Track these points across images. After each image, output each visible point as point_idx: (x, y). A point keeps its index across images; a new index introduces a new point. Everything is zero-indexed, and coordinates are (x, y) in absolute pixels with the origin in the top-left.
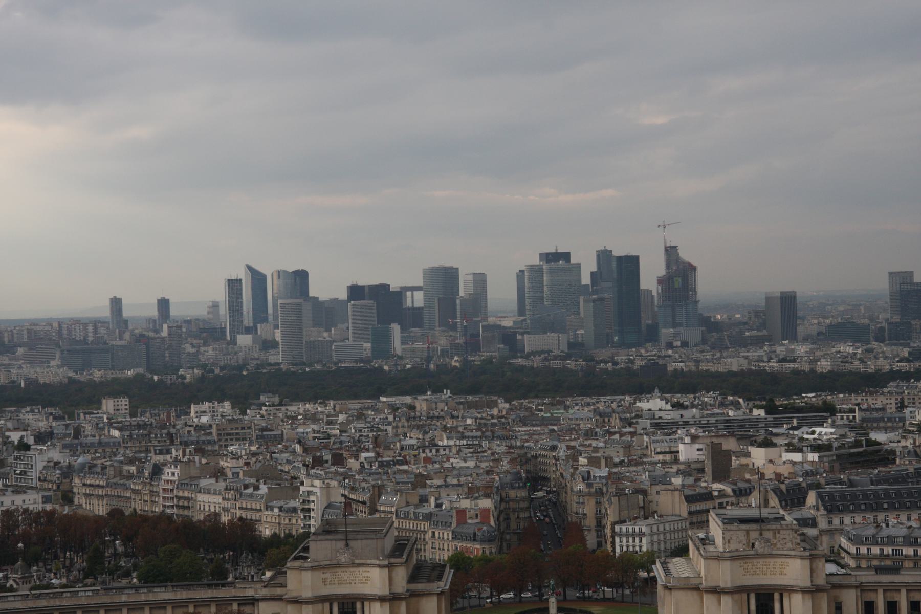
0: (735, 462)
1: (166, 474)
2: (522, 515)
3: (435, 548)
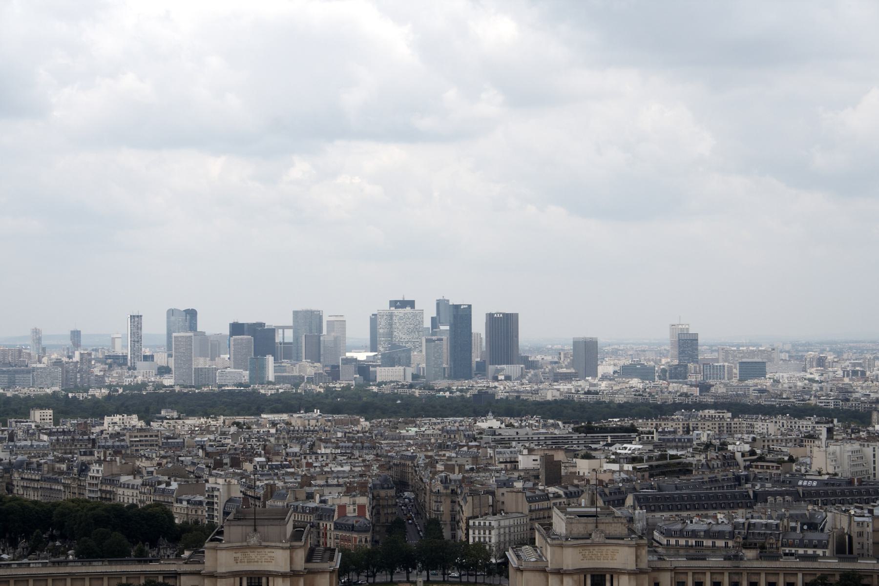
1: (92, 471)
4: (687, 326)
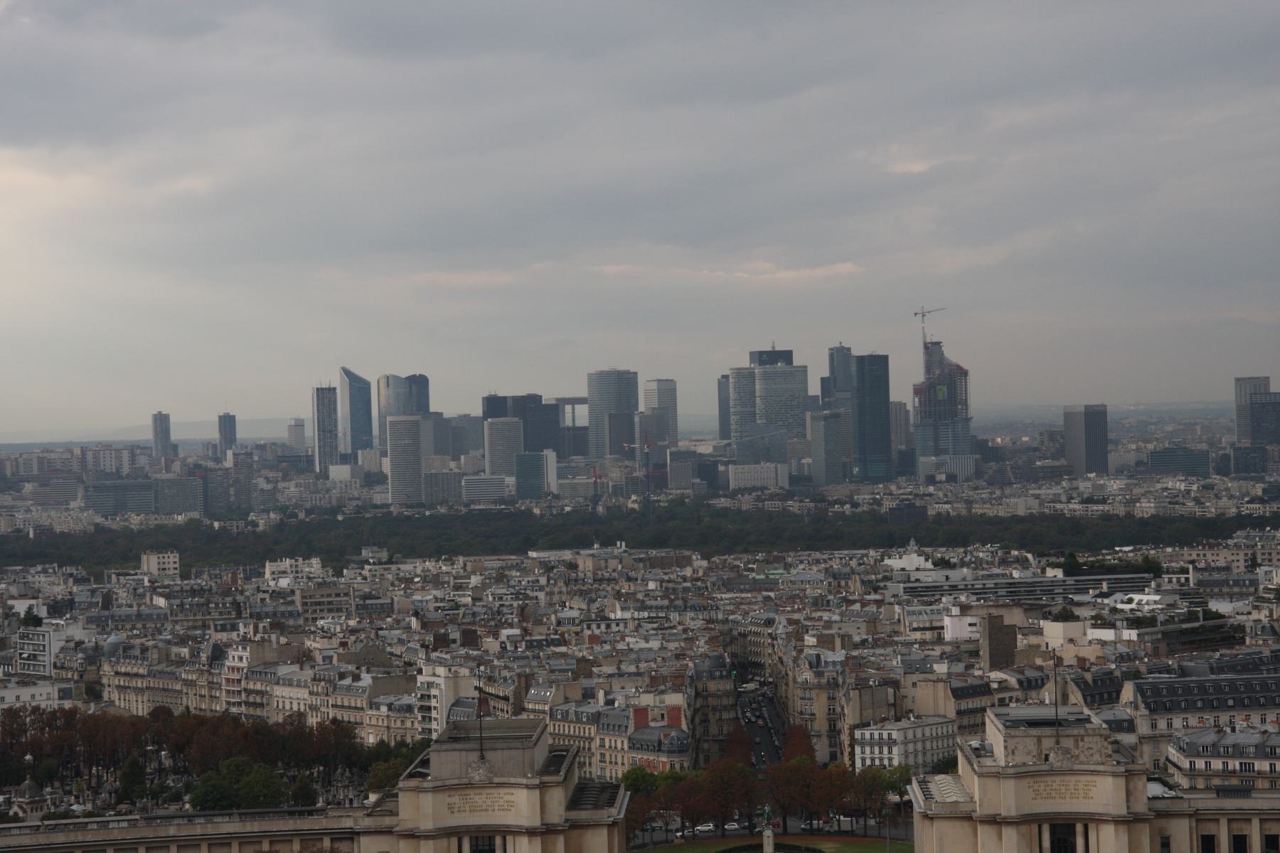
0: (1021, 642)
1: (231, 658)
2: (725, 716)
3: (605, 762)
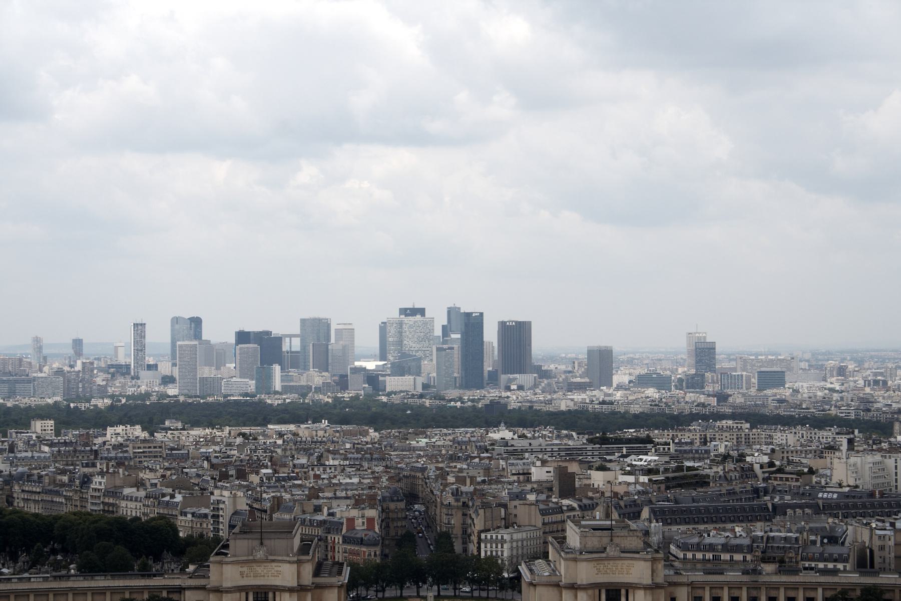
1: (94, 483)
4: (704, 335)
